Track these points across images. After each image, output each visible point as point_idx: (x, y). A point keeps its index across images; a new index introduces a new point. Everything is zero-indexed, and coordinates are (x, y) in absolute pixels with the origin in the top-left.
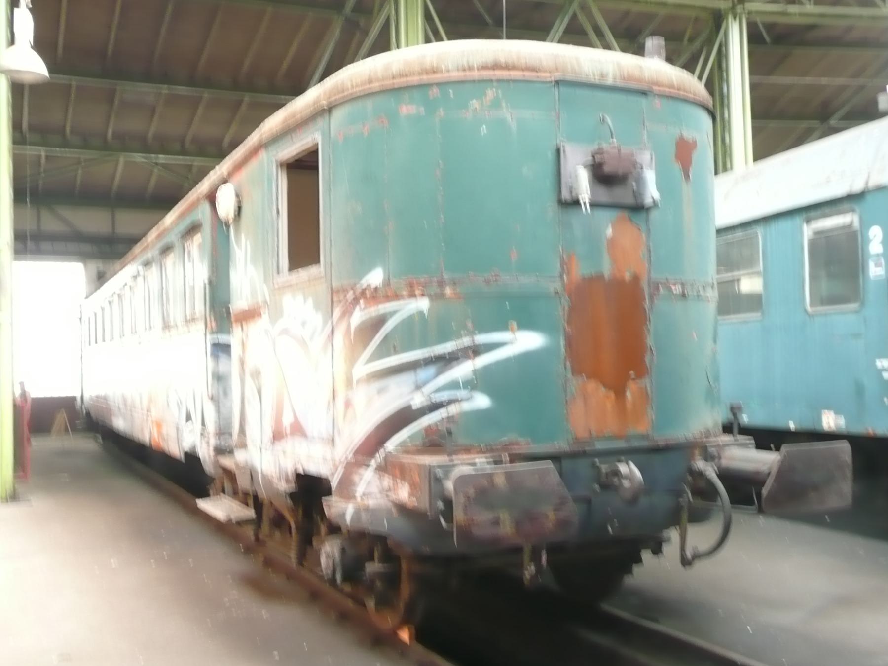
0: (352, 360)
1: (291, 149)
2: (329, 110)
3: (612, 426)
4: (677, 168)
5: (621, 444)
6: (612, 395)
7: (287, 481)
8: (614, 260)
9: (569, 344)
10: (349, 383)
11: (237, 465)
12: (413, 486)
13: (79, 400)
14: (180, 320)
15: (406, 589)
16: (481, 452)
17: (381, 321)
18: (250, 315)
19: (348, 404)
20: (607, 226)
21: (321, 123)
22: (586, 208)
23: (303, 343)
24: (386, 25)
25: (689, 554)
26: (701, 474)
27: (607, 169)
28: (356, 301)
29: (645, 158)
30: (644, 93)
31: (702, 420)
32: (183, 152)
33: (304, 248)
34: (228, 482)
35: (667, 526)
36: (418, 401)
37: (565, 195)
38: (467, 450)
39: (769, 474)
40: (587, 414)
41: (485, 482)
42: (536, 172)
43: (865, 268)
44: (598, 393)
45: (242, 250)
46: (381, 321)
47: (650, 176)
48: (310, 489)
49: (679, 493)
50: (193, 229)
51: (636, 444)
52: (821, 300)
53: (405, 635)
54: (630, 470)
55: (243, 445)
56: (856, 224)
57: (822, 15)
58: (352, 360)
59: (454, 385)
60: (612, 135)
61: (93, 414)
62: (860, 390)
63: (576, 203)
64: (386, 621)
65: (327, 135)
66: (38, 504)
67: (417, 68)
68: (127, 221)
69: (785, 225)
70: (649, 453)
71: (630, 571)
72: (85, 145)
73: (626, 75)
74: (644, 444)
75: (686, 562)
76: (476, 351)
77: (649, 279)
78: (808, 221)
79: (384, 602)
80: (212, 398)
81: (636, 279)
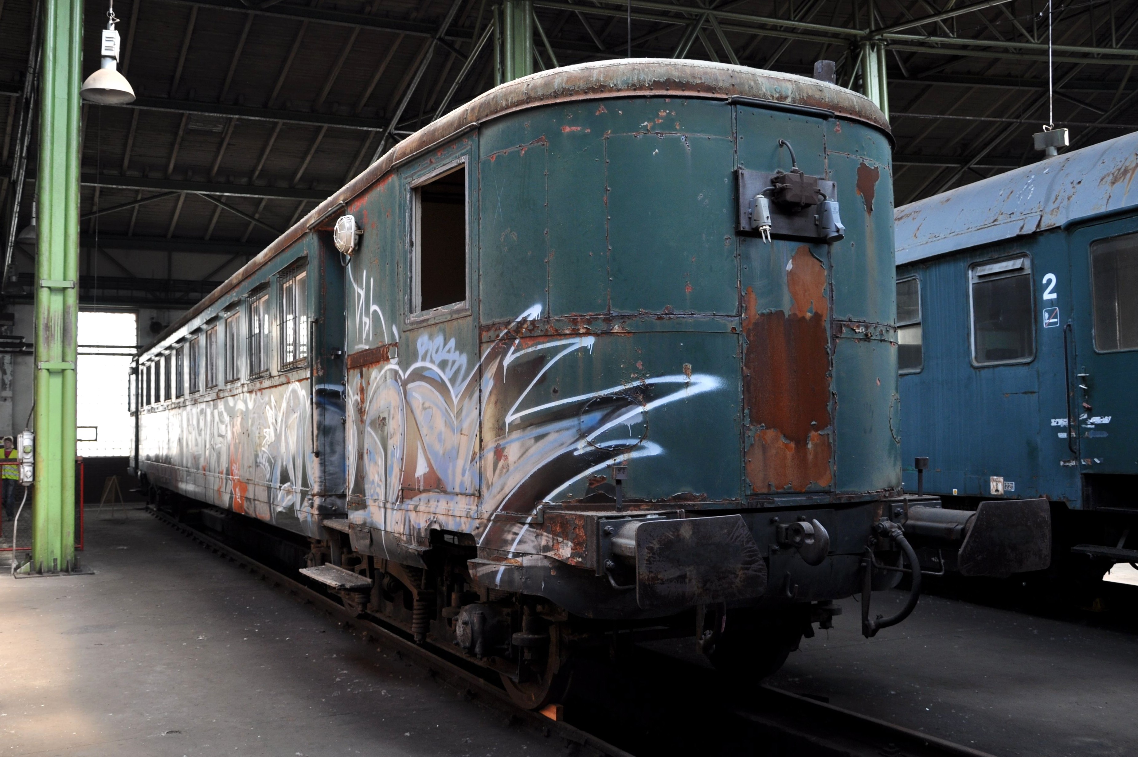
0: (503, 407)
1: (428, 174)
2: (480, 128)
3: (792, 478)
4: (859, 198)
5: (801, 500)
6: (792, 445)
7: (420, 543)
8: (794, 295)
9: (747, 389)
10: (500, 429)
11: (351, 526)
12: (578, 544)
13: (132, 463)
14: (275, 368)
15: (554, 663)
16: (654, 507)
17: (540, 359)
18: (374, 357)
19: (499, 453)
20: (788, 260)
21: (468, 144)
22: (767, 239)
23: (441, 386)
24: (489, 49)
25: (872, 621)
26: (886, 533)
27: (789, 197)
28: (509, 339)
29: (827, 186)
30: (825, 117)
31: (886, 474)
32: (250, 188)
33: (443, 281)
34: (338, 546)
35: (841, 594)
36: (581, 448)
37: (744, 225)
38: (637, 503)
39: (963, 532)
40: (769, 464)
41: (670, 535)
42: (712, 199)
43: (1038, 319)
44: (779, 444)
45: (361, 289)
46: (540, 359)
47: (834, 205)
48: (447, 553)
49: (864, 555)
50: (298, 264)
51: (817, 499)
52: (989, 354)
53: (551, 714)
54: (813, 526)
55: (362, 505)
56: (1028, 271)
57: (964, 47)
58: (503, 407)
59: (621, 431)
60: (794, 162)
61: (151, 479)
62: (1032, 451)
63: (755, 233)
64: (528, 698)
65: (475, 157)
66: (103, 576)
67: (582, 85)
68: (190, 265)
69: (947, 269)
70: (832, 509)
71: (794, 645)
72: (144, 180)
73: (805, 95)
74: (827, 499)
75: (869, 632)
76: (649, 393)
77: (832, 321)
78: (974, 266)
79: (530, 676)
80: (317, 454)
81: (817, 317)
